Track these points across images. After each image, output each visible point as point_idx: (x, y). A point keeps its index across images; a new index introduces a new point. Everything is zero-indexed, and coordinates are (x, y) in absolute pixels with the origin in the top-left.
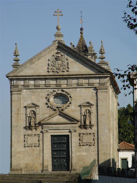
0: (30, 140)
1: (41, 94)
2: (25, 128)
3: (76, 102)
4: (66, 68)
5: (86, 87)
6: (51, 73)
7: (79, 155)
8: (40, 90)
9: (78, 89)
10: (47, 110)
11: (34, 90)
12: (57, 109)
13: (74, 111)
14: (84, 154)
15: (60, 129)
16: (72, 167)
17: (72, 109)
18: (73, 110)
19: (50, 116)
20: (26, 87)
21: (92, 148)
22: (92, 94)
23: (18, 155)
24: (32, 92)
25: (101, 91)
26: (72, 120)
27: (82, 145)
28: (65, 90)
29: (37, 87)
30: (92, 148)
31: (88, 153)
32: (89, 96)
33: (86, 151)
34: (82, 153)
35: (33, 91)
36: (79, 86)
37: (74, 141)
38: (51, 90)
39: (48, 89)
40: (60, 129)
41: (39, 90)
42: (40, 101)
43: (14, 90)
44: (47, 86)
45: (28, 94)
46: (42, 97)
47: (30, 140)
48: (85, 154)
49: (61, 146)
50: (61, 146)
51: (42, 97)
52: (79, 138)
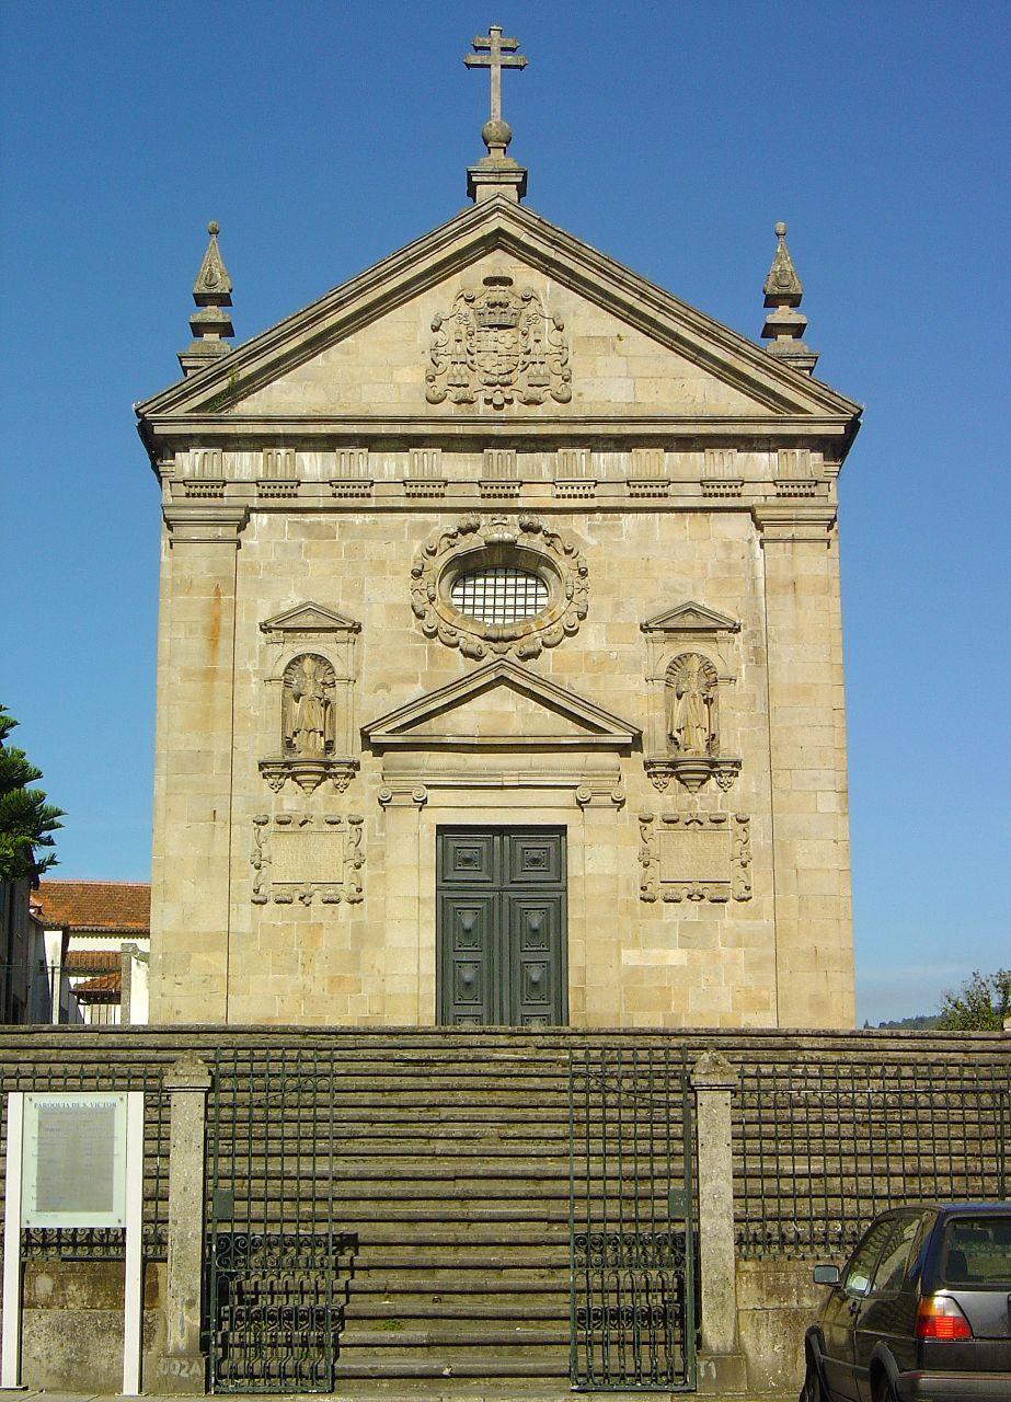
0: (289, 860)
1: (374, 548)
2: (281, 770)
3: (618, 606)
4: (556, 381)
5: (680, 503)
6: (447, 409)
7: (635, 969)
8: (370, 517)
9: (627, 520)
10: (416, 652)
11: (323, 518)
12: (485, 647)
13: (600, 665)
14: (670, 962)
15: (502, 787)
16: (770, 1120)
17: (588, 654)
18: (609, 663)
19: (213, 634)
20: (281, 497)
21: (728, 922)
22: (722, 556)
23: (204, 957)
24: (310, 531)
25: (789, 535)
26: (596, 734)
27: (659, 895)
28: (546, 521)
29: (350, 499)
30: (728, 922)
31: (698, 953)
32: (704, 567)
33: (688, 937)
34: (655, 951)
35: (319, 523)
36: (650, 499)
37: (598, 862)
38: (449, 523)
39: (419, 517)
40: (502, 787)
41: (358, 518)
42: (361, 592)
43: (167, 396)
44: (421, 497)
45: (285, 548)
46: (380, 566)
47: (289, 860)
48: (676, 957)
49: (502, 900)
50: (502, 900)
51: (380, 566)
52: (271, 905)
